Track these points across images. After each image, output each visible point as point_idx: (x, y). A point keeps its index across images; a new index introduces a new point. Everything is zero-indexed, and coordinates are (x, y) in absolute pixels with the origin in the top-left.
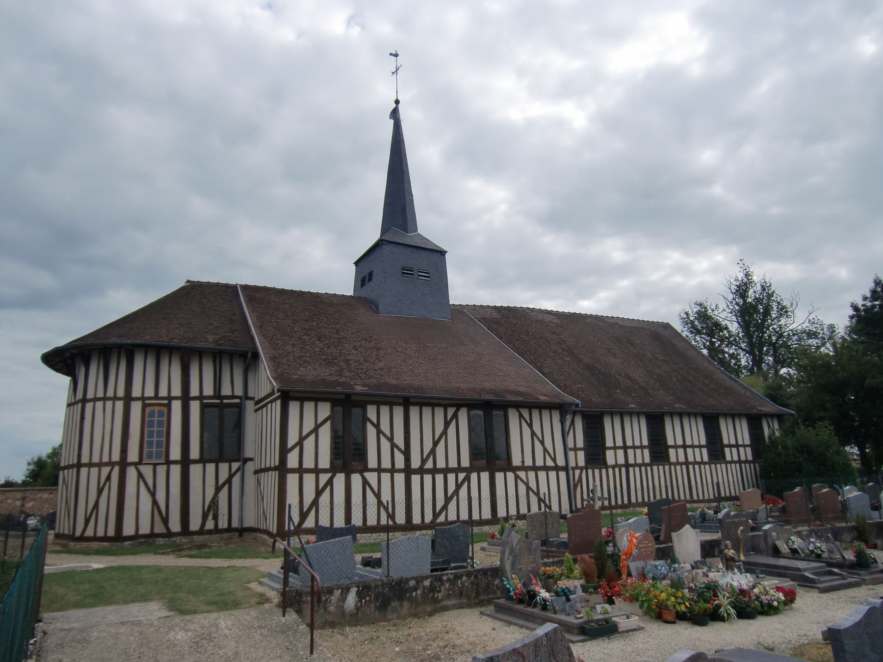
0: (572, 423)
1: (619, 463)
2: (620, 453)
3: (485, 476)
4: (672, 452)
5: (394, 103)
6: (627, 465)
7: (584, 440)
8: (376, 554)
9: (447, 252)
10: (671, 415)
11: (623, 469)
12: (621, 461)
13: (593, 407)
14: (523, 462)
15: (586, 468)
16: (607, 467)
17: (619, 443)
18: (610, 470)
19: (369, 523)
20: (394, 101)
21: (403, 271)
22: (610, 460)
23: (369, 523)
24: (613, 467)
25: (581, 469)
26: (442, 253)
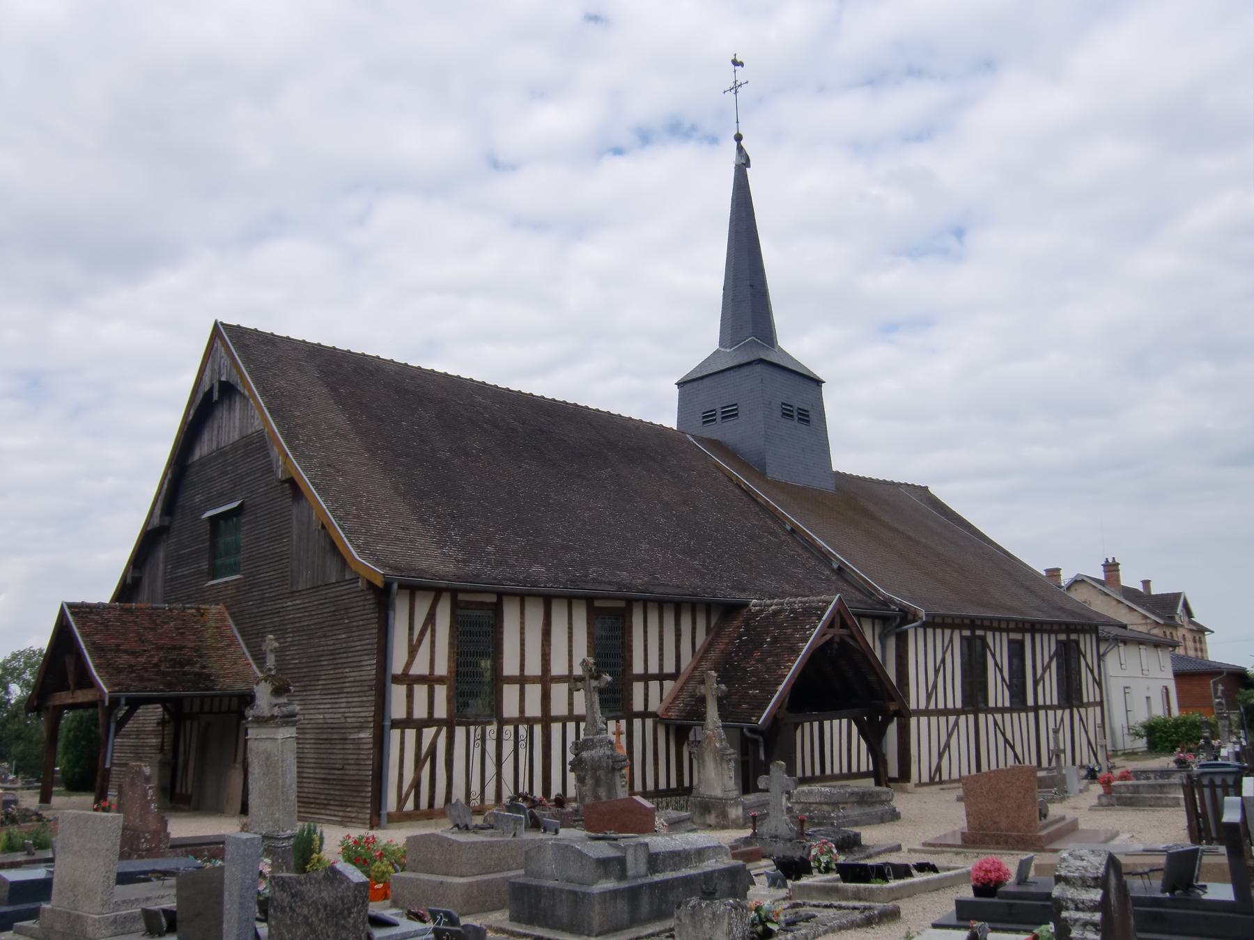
0: (431, 619)
1: (528, 714)
2: (534, 692)
3: (971, 717)
4: (510, 694)
5: (734, 141)
6: (547, 719)
7: (449, 652)
8: (226, 876)
9: (824, 382)
10: (522, 597)
11: (538, 729)
12: (533, 709)
13: (428, 577)
14: (1095, 699)
15: (450, 724)
16: (502, 722)
17: (534, 668)
18: (508, 729)
19: (862, 770)
20: (733, 136)
21: (783, 406)
22: (510, 708)
23: (862, 770)
24: (516, 722)
25: (439, 723)
26: (818, 382)
